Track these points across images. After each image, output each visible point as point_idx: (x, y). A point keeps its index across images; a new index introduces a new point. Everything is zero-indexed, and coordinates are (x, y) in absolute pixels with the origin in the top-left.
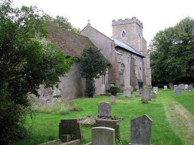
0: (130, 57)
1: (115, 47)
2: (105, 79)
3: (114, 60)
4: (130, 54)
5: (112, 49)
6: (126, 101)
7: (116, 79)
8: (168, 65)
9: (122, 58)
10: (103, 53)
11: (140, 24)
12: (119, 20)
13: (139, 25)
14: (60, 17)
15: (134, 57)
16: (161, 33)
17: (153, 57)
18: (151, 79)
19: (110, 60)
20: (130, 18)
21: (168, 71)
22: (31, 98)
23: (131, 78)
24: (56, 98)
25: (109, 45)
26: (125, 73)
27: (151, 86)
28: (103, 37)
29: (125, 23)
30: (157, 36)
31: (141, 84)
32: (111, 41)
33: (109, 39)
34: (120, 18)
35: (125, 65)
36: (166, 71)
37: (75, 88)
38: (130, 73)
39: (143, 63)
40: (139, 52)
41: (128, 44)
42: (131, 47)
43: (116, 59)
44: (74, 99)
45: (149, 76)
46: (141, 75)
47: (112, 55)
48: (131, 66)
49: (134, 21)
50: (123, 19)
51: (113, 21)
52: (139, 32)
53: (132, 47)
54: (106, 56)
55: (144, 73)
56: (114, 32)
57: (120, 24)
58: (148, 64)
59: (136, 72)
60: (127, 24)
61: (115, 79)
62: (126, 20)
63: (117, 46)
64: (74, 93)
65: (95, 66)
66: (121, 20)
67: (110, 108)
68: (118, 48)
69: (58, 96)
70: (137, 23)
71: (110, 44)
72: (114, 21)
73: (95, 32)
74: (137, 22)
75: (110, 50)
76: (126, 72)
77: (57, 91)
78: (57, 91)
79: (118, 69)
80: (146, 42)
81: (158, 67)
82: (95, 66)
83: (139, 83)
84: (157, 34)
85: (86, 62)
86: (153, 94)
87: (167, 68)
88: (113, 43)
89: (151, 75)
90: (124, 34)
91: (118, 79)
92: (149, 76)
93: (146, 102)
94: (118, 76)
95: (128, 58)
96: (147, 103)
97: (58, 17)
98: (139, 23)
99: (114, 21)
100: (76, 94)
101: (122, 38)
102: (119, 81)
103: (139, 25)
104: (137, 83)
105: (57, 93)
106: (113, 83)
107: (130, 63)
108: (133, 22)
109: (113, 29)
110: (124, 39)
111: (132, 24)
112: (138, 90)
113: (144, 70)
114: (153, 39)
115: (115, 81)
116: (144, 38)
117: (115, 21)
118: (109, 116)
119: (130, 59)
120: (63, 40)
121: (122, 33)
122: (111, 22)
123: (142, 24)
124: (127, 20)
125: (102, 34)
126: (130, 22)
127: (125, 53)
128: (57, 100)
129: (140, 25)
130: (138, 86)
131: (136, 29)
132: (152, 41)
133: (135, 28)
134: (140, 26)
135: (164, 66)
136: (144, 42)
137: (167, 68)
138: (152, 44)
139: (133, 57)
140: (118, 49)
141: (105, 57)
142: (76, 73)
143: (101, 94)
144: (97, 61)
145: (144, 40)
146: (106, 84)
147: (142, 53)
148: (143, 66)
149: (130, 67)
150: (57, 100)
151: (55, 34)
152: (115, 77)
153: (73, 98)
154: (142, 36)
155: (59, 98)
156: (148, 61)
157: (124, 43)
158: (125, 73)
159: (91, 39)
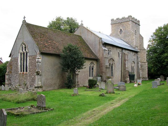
0: (121, 52)
1: (103, 44)
2: (93, 72)
3: (101, 55)
4: (121, 50)
5: (100, 45)
6: (94, 93)
7: (103, 72)
8: (166, 59)
9: (111, 54)
10: (93, 49)
11: (136, 22)
12: (117, 19)
13: (135, 23)
14: (69, 18)
15: (126, 52)
16: (160, 29)
17: (152, 50)
18: (147, 72)
19: (98, 55)
20: (126, 16)
21: (165, 64)
22: (16, 88)
23: (121, 71)
24: (37, 89)
25: (97, 42)
26: (115, 66)
27: (147, 78)
28: (93, 35)
29: (122, 21)
30: (156, 32)
31: (132, 77)
32: (99, 39)
33: (97, 37)
34: (118, 17)
35: (115, 60)
36: (163, 65)
37: (58, 80)
38: (121, 66)
39: (137, 57)
40: (134, 48)
41: (125, 40)
42: (127, 43)
43: (103, 55)
44: (57, 89)
45: (146, 69)
46: (135, 68)
47: (100, 51)
48: (122, 61)
49: (129, 20)
50: (121, 18)
51: (112, 20)
52: (136, 29)
53: (128, 43)
54: (95, 52)
55: (138, 66)
56: (112, 30)
57: (118, 22)
58: (145, 58)
59: (126, 66)
60: (123, 22)
61: (102, 72)
62: (123, 18)
63: (104, 43)
64: (58, 85)
65: (72, 62)
66: (119, 19)
67: (44, 99)
68: (106, 44)
69: (39, 87)
70: (132, 21)
71: (98, 41)
72: (112, 20)
73: (86, 31)
74: (133, 20)
75: (98, 46)
76: (116, 66)
77: (38, 82)
78: (38, 82)
79: (105, 63)
80: (143, 38)
81: (156, 61)
82: (72, 62)
83: (129, 75)
84: (157, 30)
85: (65, 58)
86: (124, 87)
87: (164, 61)
88: (101, 41)
89: (147, 68)
90: (121, 31)
91: (104, 73)
92: (146, 69)
93: (103, 95)
94: (104, 69)
95: (119, 53)
96: (104, 96)
97: (68, 18)
98: (135, 21)
99: (112, 20)
100: (59, 85)
101: (120, 34)
102: (105, 73)
103: (135, 23)
104: (127, 75)
105: (38, 84)
106: (100, 76)
107: (121, 57)
108: (128, 20)
109: (112, 27)
110: (121, 36)
111: (128, 22)
112: (128, 82)
113: (138, 63)
114: (153, 35)
115: (102, 74)
116: (141, 34)
117: (113, 20)
118: (43, 106)
119: (121, 54)
120: (50, 40)
121: (120, 30)
122: (111, 21)
123: (139, 21)
124: (124, 18)
125: (92, 33)
126: (127, 21)
127: (115, 49)
128: (38, 90)
129: (137, 23)
130: (128, 79)
131: (132, 26)
132: (152, 36)
133: (131, 26)
134: (136, 24)
135: (162, 59)
136: (141, 38)
137: (164, 61)
138: (152, 40)
139: (125, 52)
140: (106, 46)
141: (94, 52)
142: (59, 67)
143: (83, 86)
144: (74, 57)
145: (140, 36)
146: (94, 76)
147: (136, 48)
148: (137, 60)
149: (121, 61)
150: (38, 90)
151: (43, 35)
152: (102, 71)
153: (57, 88)
154: (139, 32)
155: (39, 89)
156: (143, 57)
157: (121, 39)
158: (115, 66)
159: (83, 37)
